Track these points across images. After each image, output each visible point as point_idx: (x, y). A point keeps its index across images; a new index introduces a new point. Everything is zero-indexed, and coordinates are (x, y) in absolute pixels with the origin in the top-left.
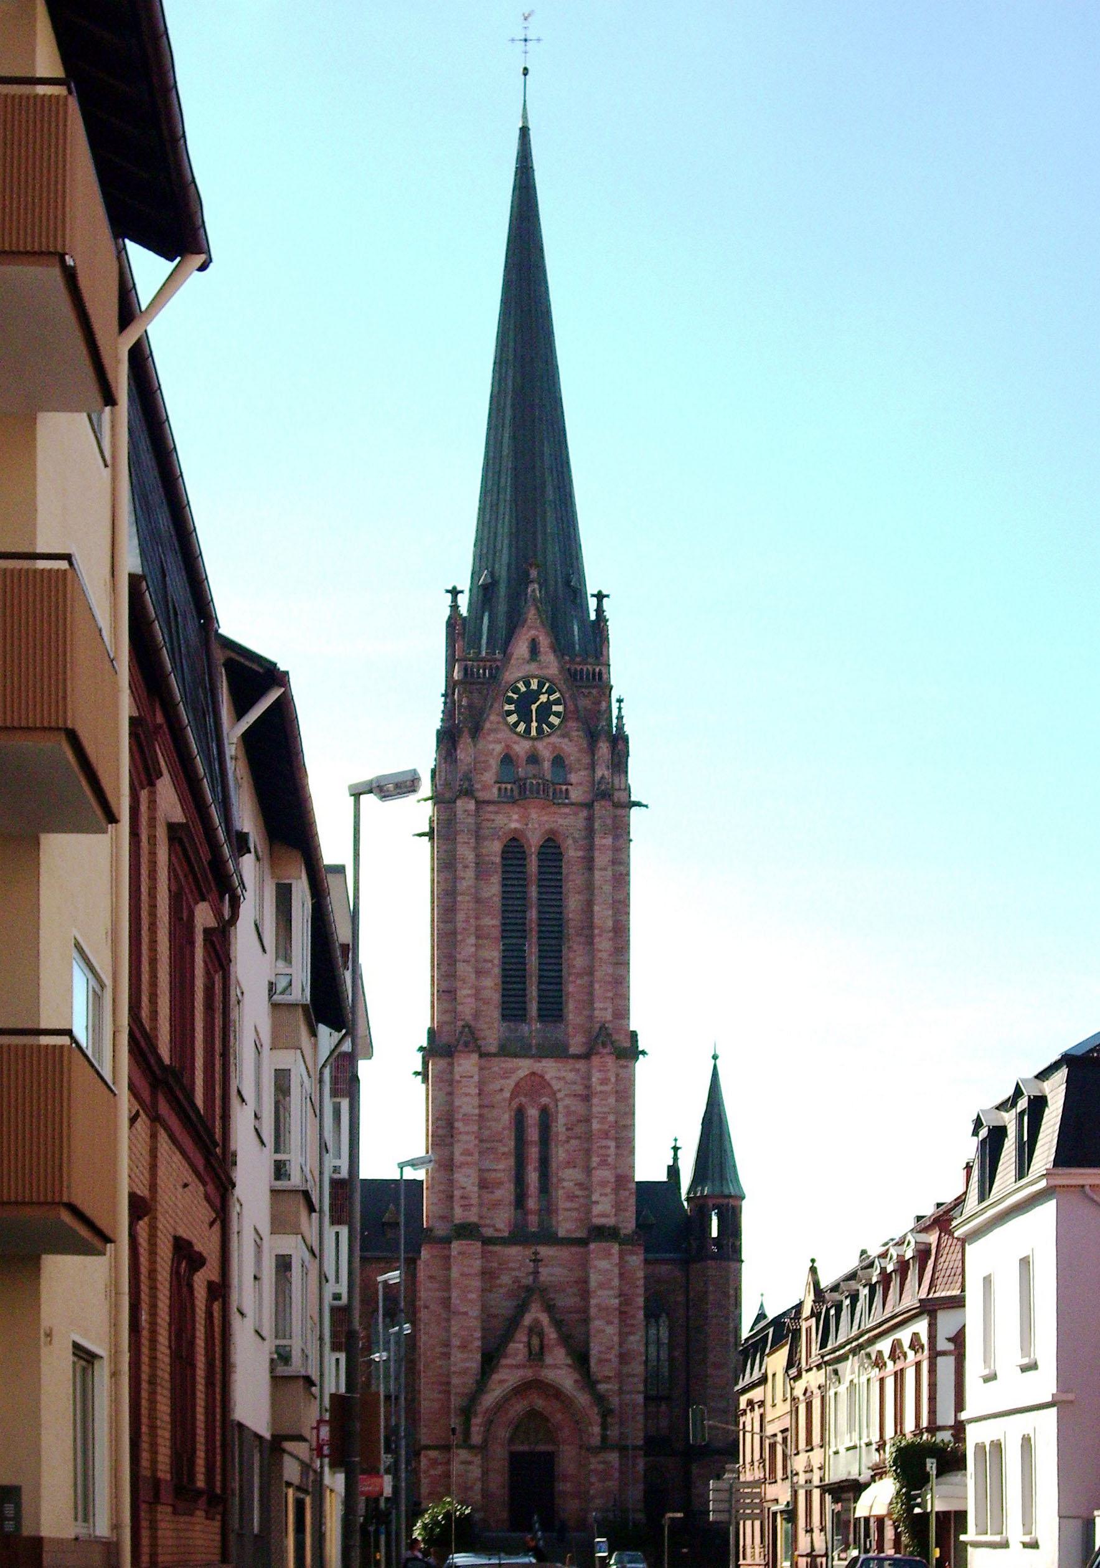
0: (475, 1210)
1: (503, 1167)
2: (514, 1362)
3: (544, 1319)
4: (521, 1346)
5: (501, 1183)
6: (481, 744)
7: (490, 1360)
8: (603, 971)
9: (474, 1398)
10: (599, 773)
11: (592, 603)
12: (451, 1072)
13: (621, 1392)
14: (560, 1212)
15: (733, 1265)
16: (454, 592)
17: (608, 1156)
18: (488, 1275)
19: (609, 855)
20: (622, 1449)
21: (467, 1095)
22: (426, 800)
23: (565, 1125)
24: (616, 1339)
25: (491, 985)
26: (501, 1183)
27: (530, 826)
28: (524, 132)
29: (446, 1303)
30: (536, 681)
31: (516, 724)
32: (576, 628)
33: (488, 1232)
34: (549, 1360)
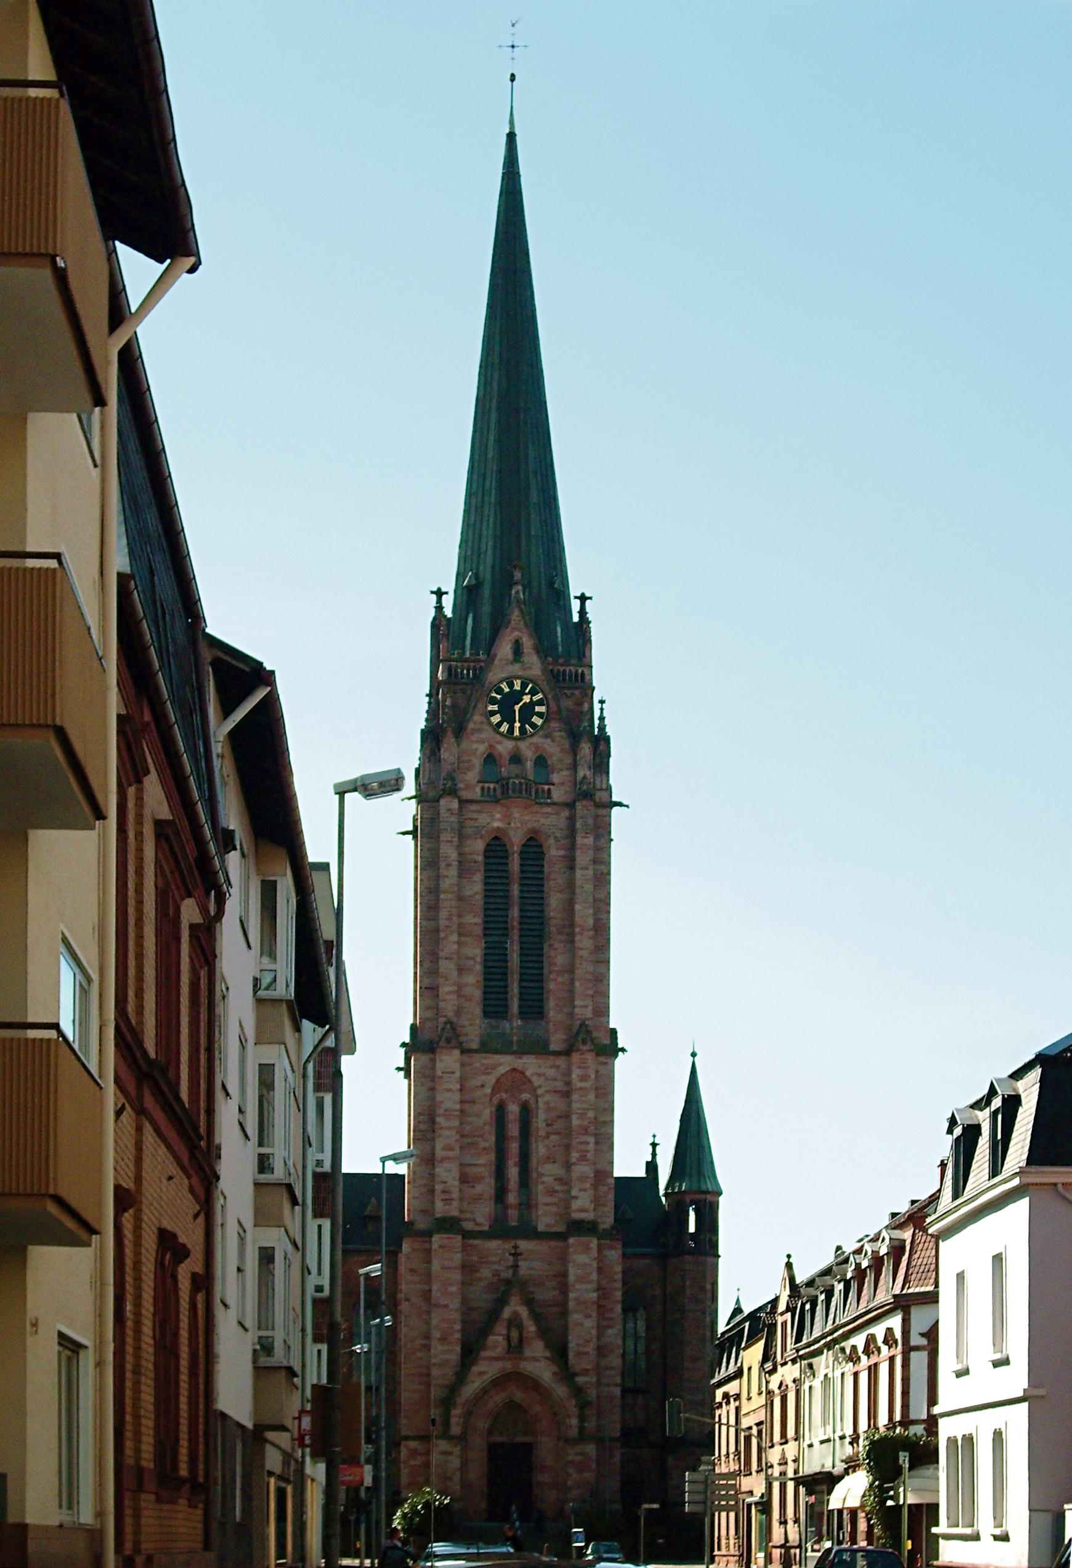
0: (455, 1204)
1: (484, 1162)
2: (493, 1355)
3: (524, 1312)
4: (500, 1338)
5: (483, 1178)
6: (465, 744)
7: (470, 1351)
8: (584, 969)
9: (454, 1389)
10: (581, 773)
11: (575, 605)
12: (433, 1068)
13: (599, 1383)
14: (540, 1206)
15: (710, 1260)
16: (439, 594)
17: (587, 1151)
18: (468, 1269)
19: (590, 854)
20: (600, 1441)
21: (448, 1090)
22: (410, 799)
23: (545, 1120)
24: (594, 1332)
25: (473, 982)
26: (483, 1178)
27: (512, 825)
28: (511, 137)
29: (427, 1296)
30: (519, 681)
31: (499, 724)
32: (559, 630)
33: (469, 1226)
34: (528, 1353)
